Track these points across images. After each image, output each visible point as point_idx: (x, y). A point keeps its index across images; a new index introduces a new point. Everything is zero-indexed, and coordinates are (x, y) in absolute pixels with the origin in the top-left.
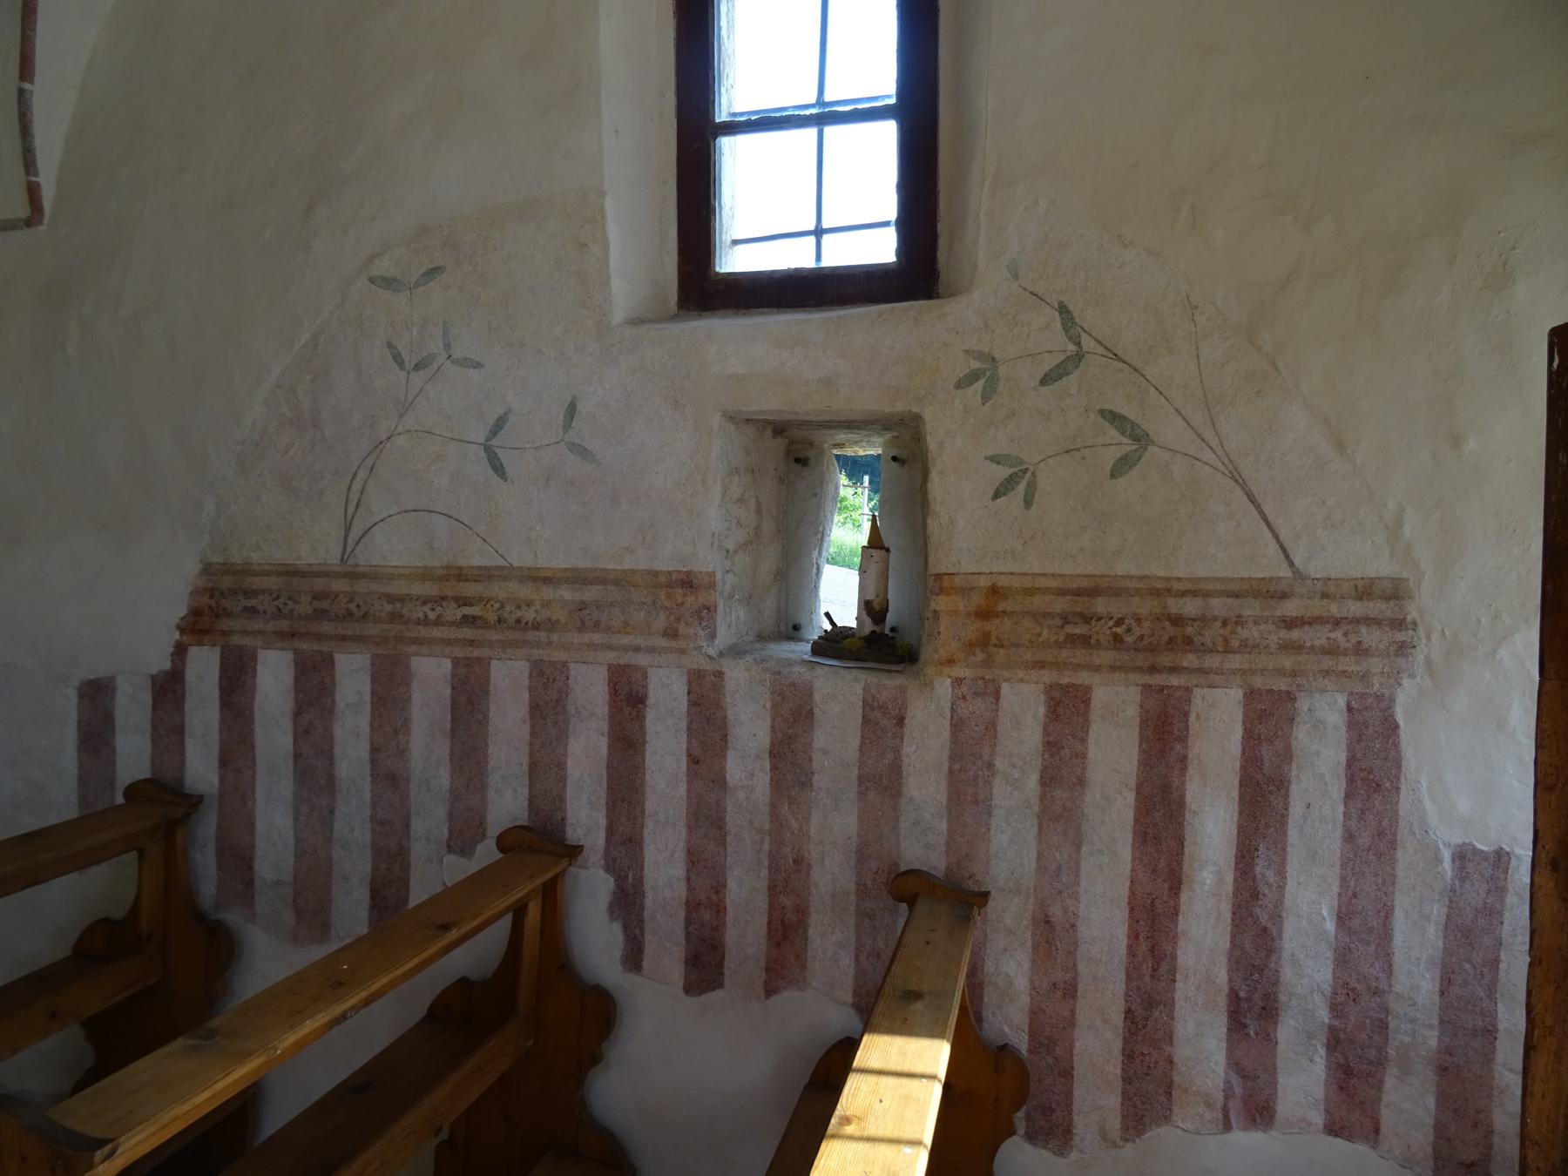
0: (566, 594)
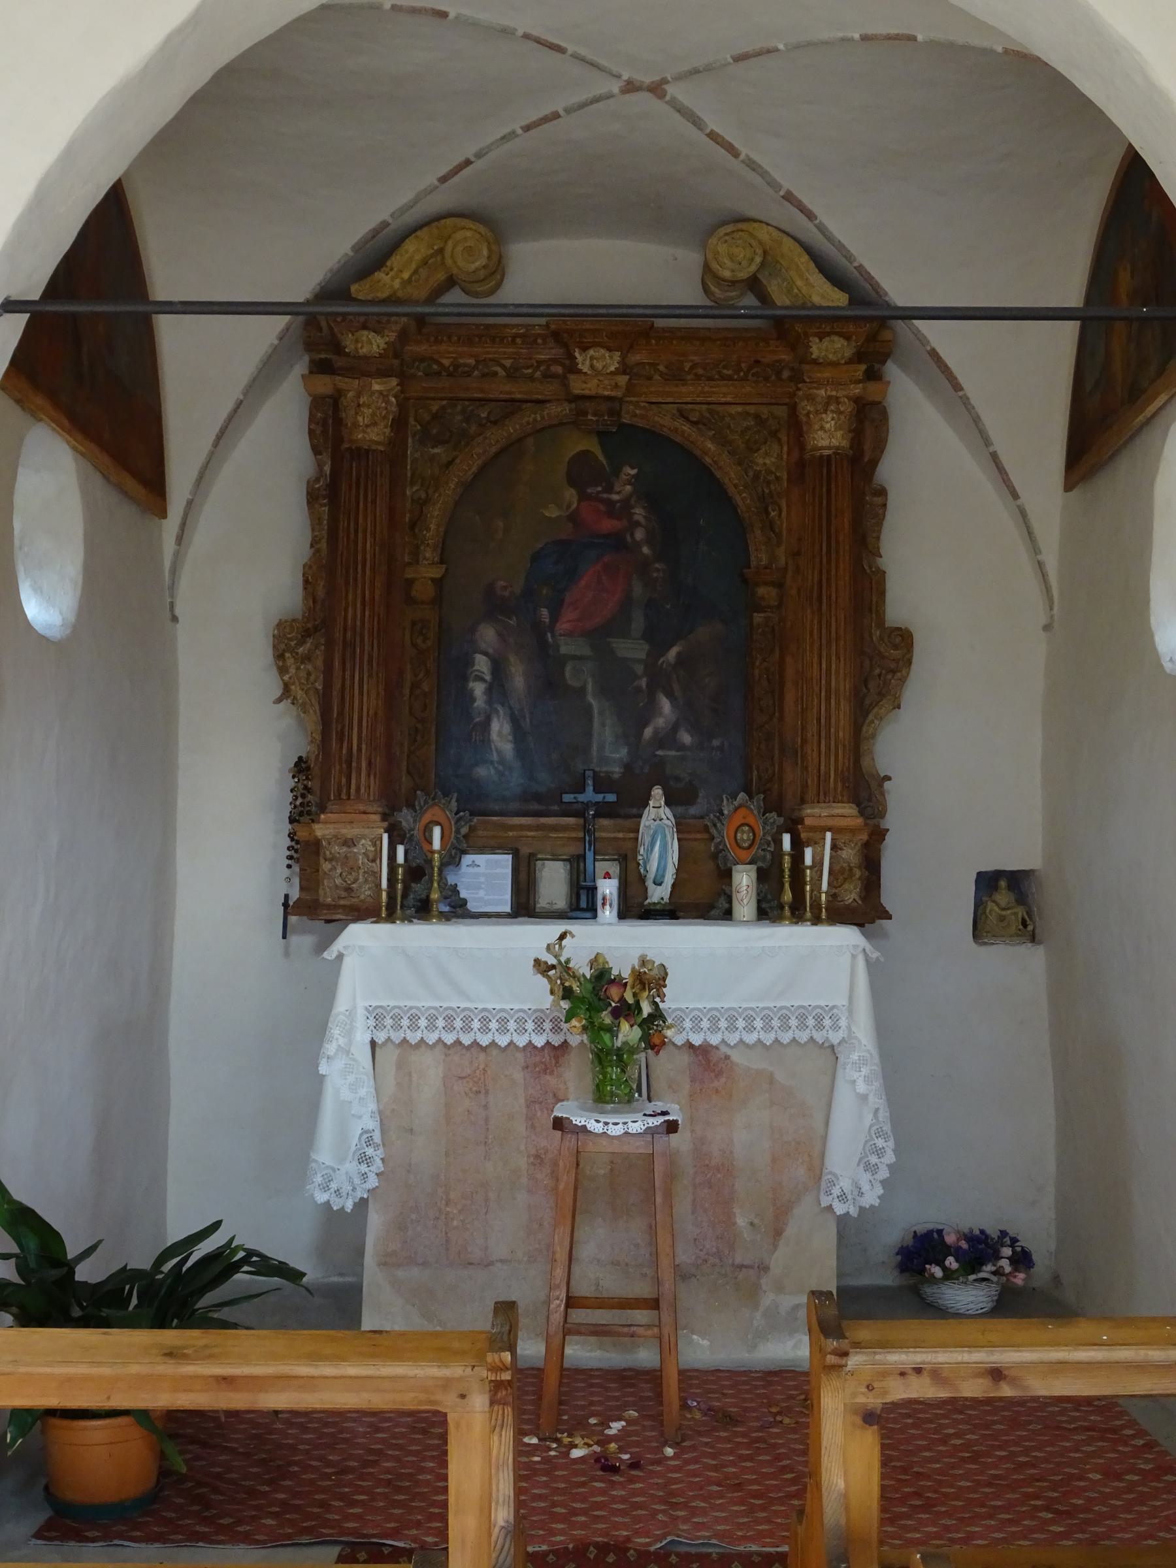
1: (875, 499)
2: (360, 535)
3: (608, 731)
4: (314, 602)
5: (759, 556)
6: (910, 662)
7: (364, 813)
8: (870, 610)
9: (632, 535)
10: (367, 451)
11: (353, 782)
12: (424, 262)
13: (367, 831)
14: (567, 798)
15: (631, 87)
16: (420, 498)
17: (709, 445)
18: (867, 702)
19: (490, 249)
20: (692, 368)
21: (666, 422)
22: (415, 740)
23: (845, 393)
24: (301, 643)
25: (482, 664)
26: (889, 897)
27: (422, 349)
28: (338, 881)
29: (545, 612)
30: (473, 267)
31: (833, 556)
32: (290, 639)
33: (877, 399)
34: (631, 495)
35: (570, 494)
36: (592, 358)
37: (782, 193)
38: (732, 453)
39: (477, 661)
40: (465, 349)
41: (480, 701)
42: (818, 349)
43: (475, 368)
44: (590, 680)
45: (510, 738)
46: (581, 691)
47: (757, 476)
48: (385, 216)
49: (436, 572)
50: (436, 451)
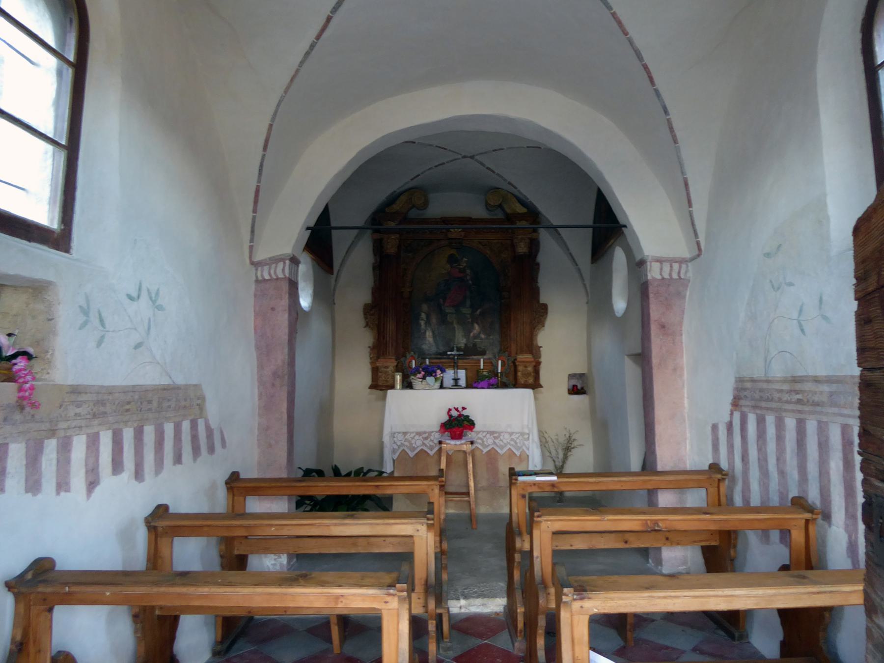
0: (826, 388)
14: (449, 353)
15: (464, 157)
25: (423, 316)
26: (542, 381)
35: (448, 266)
46: (452, 323)
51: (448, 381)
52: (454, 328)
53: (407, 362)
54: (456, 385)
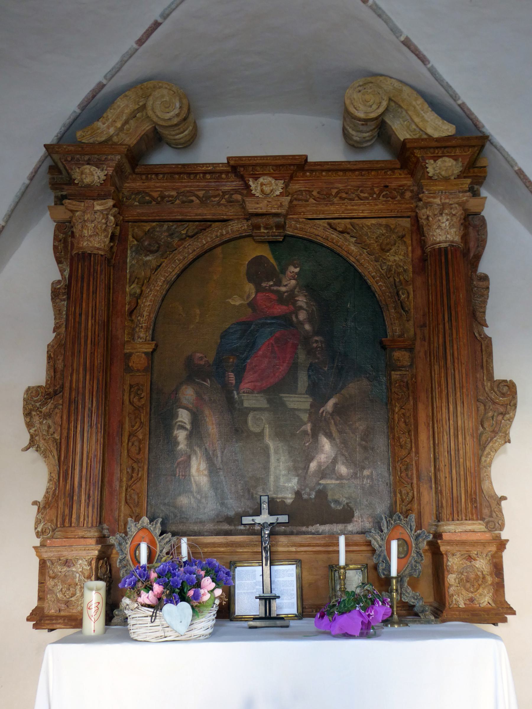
1: (481, 283)
2: (83, 317)
3: (282, 466)
4: (55, 372)
5: (394, 328)
6: (515, 405)
7: (83, 537)
8: (482, 367)
9: (297, 317)
10: (90, 255)
11: (74, 511)
12: (133, 115)
13: (84, 553)
14: (247, 520)
16: (135, 293)
17: (353, 248)
18: (484, 438)
19: (181, 102)
20: (337, 193)
21: (319, 231)
22: (132, 477)
23: (456, 200)
24: (44, 404)
27: (138, 185)
28: (60, 595)
29: (232, 375)
30: (168, 116)
31: (454, 323)
32: (36, 401)
33: (476, 210)
34: (295, 288)
35: (250, 288)
36: (262, 184)
37: (402, 39)
38: (370, 254)
39: (180, 413)
40: (168, 184)
41: (182, 446)
42: (433, 168)
43: (177, 197)
44: (267, 426)
45: (206, 472)
46: (260, 435)
47: (389, 270)
48: (98, 77)
49: (149, 348)
50: (148, 258)
51: (247, 604)
52: (266, 450)
53: (128, 547)
54: (269, 621)
